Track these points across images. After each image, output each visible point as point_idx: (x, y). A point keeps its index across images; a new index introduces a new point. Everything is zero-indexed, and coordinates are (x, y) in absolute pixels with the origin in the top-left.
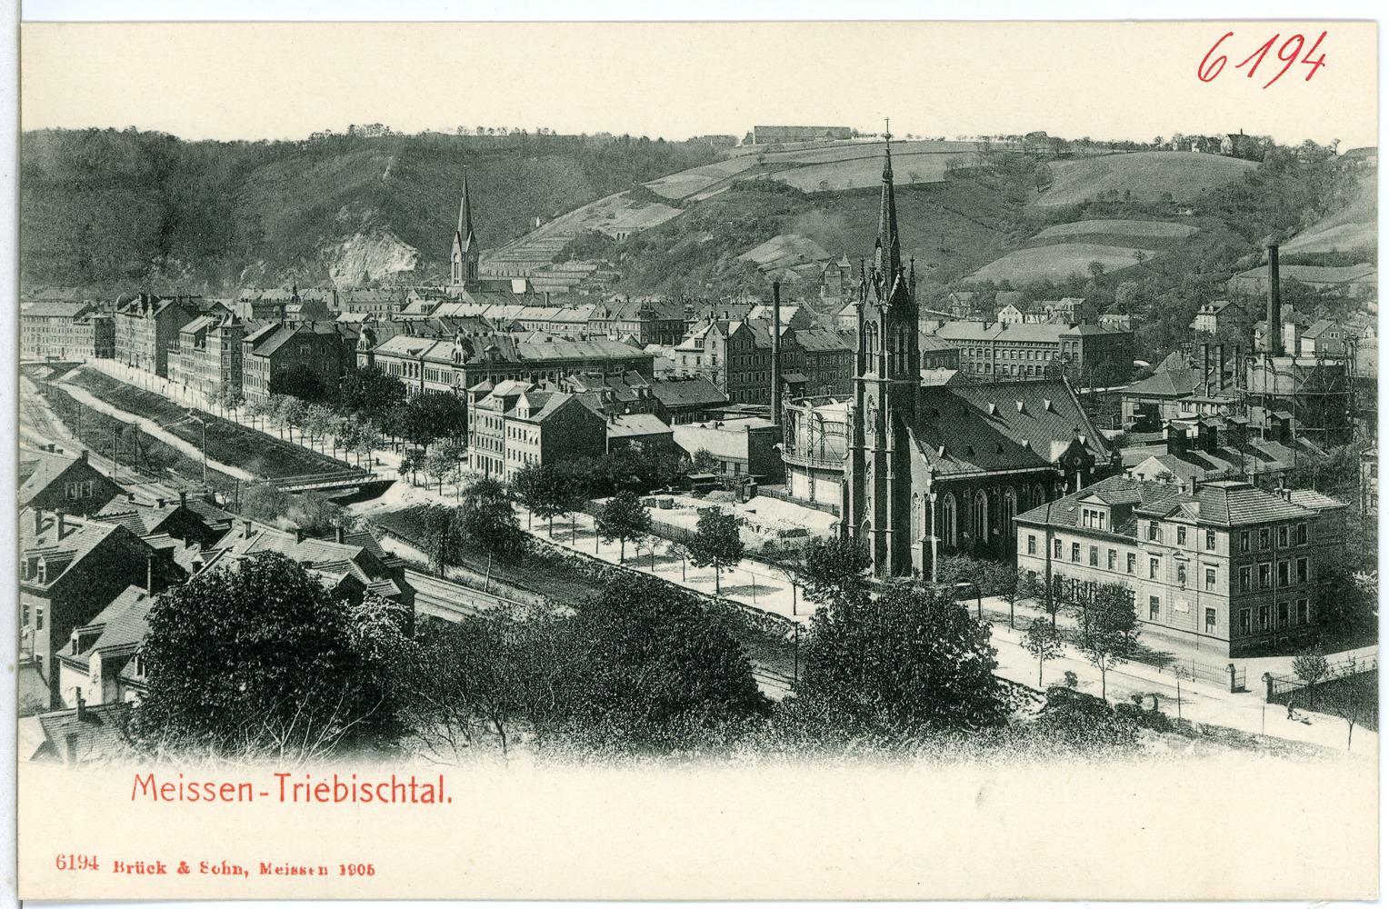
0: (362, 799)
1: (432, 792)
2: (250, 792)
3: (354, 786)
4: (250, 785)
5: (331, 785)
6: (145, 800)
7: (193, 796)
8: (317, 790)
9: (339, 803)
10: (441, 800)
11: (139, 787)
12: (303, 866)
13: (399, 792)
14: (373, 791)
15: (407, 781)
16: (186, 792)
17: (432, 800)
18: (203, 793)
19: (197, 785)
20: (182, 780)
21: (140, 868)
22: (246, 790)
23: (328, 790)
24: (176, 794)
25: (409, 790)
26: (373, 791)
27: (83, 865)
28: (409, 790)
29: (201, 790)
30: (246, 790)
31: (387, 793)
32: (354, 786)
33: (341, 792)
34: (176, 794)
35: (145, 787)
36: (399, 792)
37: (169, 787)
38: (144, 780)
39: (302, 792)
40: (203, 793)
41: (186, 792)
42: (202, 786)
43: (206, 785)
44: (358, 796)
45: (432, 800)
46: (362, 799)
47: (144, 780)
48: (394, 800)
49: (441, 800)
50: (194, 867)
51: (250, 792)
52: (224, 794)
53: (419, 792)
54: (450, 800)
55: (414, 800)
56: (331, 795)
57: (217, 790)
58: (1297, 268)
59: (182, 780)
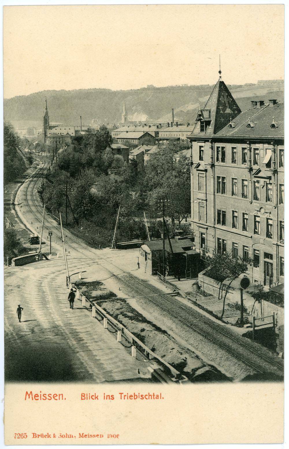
0: (43, 399)
1: (158, 396)
2: (62, 397)
3: (41, 395)
4: (62, 395)
5: (133, 396)
6: (29, 400)
7: (45, 398)
8: (35, 397)
9: (83, 400)
10: (161, 398)
11: (28, 396)
12: (94, 434)
13: (150, 397)
14: (144, 397)
15: (152, 394)
16: (42, 397)
17: (158, 398)
18: (48, 397)
19: (46, 395)
20: (41, 393)
21: (42, 436)
22: (61, 396)
23: (38, 396)
24: (39, 398)
25: (153, 396)
26: (144, 397)
27: (22, 435)
28: (153, 396)
29: (47, 396)
30: (61, 396)
31: (147, 397)
32: (41, 395)
33: (136, 397)
34: (39, 398)
35: (29, 395)
36: (150, 397)
37: (37, 396)
38: (29, 393)
39: (126, 397)
40: (48, 397)
41: (42, 397)
42: (47, 395)
43: (49, 395)
44: (42, 398)
45: (158, 398)
46: (48, 399)
47: (29, 393)
48: (59, 399)
49: (161, 398)
50: (58, 435)
51: (62, 397)
52: (55, 398)
53: (155, 397)
54: (65, 399)
55: (154, 399)
56: (133, 398)
57: (52, 396)
58: (164, 377)
59: (41, 393)
